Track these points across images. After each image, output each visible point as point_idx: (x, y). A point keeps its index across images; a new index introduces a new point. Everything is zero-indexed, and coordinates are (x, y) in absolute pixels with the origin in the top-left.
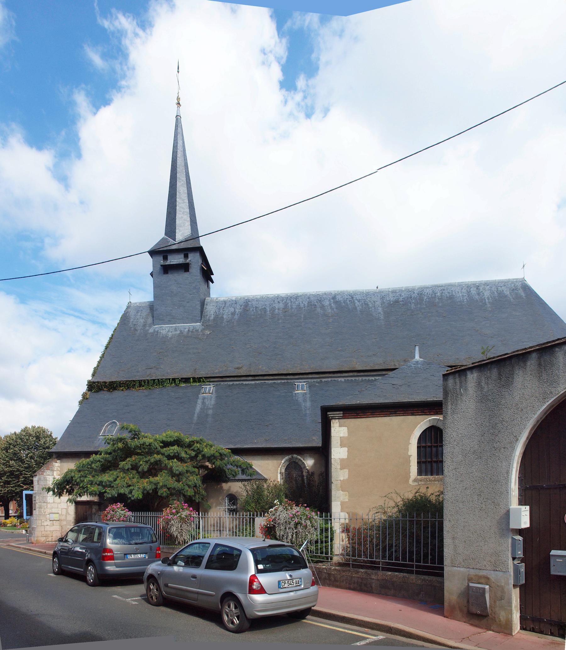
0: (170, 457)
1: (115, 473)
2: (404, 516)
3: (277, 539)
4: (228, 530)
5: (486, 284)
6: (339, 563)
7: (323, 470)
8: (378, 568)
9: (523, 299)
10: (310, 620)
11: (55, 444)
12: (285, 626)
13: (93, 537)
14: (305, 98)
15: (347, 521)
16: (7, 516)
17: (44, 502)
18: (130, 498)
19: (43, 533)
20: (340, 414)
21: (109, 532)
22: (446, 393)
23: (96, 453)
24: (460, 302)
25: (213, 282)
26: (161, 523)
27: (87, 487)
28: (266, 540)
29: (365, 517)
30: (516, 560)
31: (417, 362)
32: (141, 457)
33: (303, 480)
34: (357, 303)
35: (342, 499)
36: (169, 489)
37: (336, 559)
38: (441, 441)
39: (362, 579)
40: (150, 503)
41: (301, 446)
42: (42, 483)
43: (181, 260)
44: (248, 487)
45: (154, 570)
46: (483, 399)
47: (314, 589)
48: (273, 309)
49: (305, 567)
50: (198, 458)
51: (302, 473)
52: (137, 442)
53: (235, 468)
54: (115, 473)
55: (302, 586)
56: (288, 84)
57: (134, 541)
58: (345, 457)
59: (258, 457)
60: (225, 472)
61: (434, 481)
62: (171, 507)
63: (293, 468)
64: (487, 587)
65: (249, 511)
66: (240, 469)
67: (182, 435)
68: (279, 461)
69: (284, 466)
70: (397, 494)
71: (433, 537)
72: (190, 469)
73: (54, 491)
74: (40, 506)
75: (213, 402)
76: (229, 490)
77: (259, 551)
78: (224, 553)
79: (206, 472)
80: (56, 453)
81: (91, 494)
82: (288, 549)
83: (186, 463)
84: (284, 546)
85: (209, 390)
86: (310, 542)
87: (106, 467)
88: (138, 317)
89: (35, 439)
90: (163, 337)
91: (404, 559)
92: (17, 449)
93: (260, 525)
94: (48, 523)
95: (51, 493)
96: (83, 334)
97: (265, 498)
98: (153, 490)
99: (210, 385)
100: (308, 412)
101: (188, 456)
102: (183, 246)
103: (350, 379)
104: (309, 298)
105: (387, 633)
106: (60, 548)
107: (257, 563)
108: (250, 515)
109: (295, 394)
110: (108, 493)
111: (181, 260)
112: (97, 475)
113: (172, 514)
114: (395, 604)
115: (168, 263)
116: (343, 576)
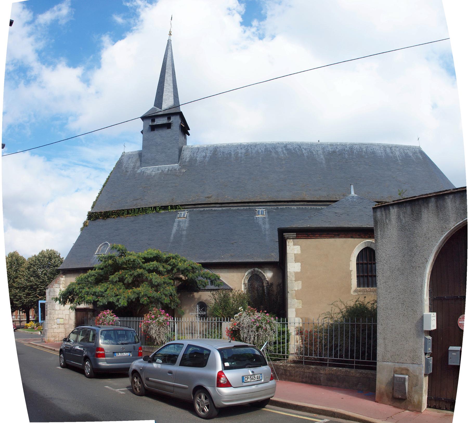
0: (150, 271)
1: (106, 285)
2: (347, 321)
3: (241, 341)
4: (198, 332)
5: (396, 147)
6: (294, 361)
7: (281, 281)
8: (326, 365)
9: (418, 161)
10: (269, 408)
11: (62, 263)
12: (247, 414)
13: (89, 338)
14: (258, 30)
15: (301, 325)
16: (28, 321)
17: (53, 310)
18: (117, 305)
19: (53, 334)
20: (294, 235)
21: (101, 334)
22: (376, 222)
23: (92, 269)
24: (380, 156)
25: (189, 135)
26: (143, 326)
27: (84, 297)
28: (232, 341)
29: (316, 321)
30: (427, 355)
31: (353, 197)
32: (127, 271)
33: (263, 290)
34: (304, 151)
35: (296, 306)
36: (149, 297)
37: (291, 357)
38: (374, 259)
39: (313, 373)
40: (133, 310)
41: (262, 260)
42: (52, 294)
43: (165, 121)
44: (216, 296)
45: (137, 366)
46: (402, 228)
47: (272, 382)
48: (237, 154)
49: (265, 364)
50: (173, 271)
51: (263, 283)
52: (123, 259)
53: (205, 280)
54: (106, 285)
55: (263, 381)
56: (246, 21)
57: (120, 342)
58: (299, 271)
59: (225, 270)
60: (196, 283)
61: (370, 291)
62: (150, 313)
63: (255, 279)
64: (407, 377)
65: (217, 316)
66: (209, 281)
67: (161, 252)
68: (243, 274)
69: (247, 278)
70: (342, 302)
71: (369, 338)
72: (166, 281)
73: (60, 300)
74: (50, 312)
75: (187, 225)
76: (200, 298)
77: (225, 351)
78: (196, 353)
79: (180, 283)
80: (62, 270)
81: (87, 302)
82: (251, 349)
83: (163, 275)
84: (247, 346)
85: (184, 215)
86: (270, 343)
87: (99, 280)
88: (129, 162)
89: (48, 259)
90: (148, 176)
91: (347, 356)
92: (35, 268)
93: (227, 328)
94: (56, 326)
95: (58, 302)
96: (88, 178)
97: (231, 305)
98: (136, 299)
99: (184, 211)
100: (267, 233)
101: (165, 270)
102: (167, 112)
103: (301, 207)
104: (265, 146)
105: (331, 417)
106: (64, 346)
107: (224, 361)
108: (218, 320)
109: (256, 218)
110: (100, 302)
111: (165, 121)
112: (92, 287)
113: (152, 319)
114: (338, 393)
115: (155, 123)
116: (297, 371)
